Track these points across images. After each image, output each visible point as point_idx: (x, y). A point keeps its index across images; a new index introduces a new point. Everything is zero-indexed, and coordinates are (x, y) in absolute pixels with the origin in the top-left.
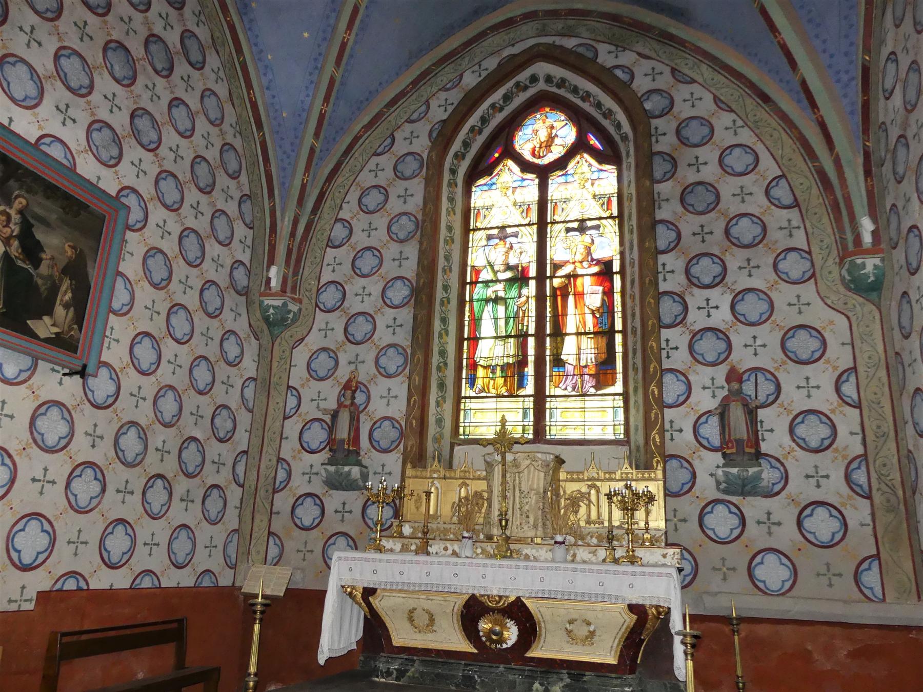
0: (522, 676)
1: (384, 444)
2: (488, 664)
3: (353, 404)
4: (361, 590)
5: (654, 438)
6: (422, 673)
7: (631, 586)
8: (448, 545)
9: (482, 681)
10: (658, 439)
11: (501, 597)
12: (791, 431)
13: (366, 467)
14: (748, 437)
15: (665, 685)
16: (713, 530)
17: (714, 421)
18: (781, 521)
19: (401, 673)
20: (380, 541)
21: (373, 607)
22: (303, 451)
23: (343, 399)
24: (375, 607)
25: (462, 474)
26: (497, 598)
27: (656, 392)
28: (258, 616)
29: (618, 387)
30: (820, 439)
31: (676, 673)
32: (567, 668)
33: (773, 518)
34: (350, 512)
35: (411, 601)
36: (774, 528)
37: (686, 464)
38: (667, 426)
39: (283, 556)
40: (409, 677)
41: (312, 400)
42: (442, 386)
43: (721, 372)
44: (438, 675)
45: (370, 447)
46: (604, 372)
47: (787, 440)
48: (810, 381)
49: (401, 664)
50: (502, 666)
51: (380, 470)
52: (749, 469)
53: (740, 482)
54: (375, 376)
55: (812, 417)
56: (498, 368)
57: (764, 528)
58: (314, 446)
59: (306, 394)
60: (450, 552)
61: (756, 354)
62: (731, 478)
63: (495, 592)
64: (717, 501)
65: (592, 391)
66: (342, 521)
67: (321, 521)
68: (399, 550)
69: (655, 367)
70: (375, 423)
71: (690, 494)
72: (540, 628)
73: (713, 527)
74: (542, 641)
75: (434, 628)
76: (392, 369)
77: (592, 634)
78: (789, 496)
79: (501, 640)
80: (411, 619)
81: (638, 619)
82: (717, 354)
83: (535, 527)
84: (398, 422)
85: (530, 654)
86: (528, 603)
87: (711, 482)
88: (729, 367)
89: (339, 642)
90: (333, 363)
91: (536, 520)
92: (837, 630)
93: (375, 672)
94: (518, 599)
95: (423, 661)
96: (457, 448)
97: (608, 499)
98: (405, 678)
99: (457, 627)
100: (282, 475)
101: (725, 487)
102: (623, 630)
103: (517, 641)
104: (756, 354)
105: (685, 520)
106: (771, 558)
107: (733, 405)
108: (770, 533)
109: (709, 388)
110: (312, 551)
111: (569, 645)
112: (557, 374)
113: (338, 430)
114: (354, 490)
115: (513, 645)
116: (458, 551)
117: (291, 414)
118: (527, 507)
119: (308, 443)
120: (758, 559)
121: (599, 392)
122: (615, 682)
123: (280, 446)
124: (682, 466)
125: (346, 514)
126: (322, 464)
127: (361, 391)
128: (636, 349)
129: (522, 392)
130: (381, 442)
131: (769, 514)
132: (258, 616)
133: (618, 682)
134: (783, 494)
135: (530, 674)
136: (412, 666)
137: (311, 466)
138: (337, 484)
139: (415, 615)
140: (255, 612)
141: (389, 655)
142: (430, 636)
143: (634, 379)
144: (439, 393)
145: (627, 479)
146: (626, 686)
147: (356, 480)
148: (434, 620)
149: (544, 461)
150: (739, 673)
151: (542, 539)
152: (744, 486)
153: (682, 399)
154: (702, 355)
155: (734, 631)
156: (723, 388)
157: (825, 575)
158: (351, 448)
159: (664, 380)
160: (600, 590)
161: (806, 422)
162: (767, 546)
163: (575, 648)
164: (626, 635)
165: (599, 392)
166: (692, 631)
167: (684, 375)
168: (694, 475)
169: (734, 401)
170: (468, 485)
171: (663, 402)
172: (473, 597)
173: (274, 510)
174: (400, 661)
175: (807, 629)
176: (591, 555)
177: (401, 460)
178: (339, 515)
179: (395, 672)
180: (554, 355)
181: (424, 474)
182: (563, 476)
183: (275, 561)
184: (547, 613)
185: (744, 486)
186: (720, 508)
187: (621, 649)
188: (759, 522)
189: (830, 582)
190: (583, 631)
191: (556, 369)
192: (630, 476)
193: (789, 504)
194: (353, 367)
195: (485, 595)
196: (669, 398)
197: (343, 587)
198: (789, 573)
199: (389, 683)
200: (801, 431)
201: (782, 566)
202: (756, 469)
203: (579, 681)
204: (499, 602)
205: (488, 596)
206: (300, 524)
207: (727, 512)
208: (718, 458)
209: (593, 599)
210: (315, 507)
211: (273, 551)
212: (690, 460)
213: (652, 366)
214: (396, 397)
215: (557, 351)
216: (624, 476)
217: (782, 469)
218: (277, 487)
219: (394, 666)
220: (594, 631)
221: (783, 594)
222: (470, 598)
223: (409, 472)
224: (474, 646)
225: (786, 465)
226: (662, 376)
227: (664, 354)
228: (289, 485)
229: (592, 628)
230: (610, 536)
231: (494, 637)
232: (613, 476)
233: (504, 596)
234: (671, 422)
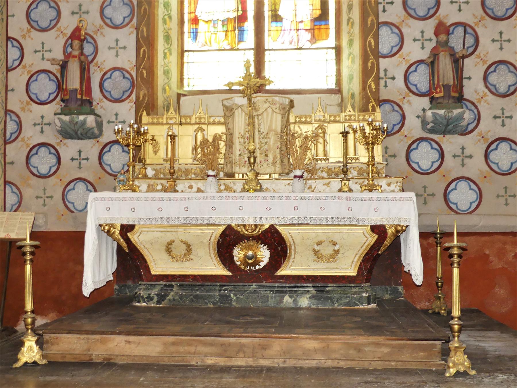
0: (273, 291)
1: (116, 94)
2: (241, 284)
3: (82, 54)
4: (119, 228)
5: (370, 85)
6: (181, 297)
7: (376, 209)
8: (193, 184)
9: (238, 298)
10: (373, 86)
11: (256, 226)
12: (485, 78)
13: (100, 117)
14: (454, 82)
15: (387, 289)
16: (418, 163)
17: (423, 70)
18: (473, 155)
19: (161, 298)
20: (133, 181)
21: (131, 242)
22: (32, 102)
23: (69, 50)
24: (133, 242)
25: (198, 120)
26: (253, 227)
27: (373, 44)
28: (28, 257)
29: (331, 41)
30: (507, 86)
31: (414, 279)
32: (313, 282)
33: (467, 152)
34: (87, 159)
35: (168, 234)
36: (466, 161)
37: (397, 108)
38: (382, 74)
39: (23, 203)
40: (169, 300)
41: (36, 52)
42: (167, 38)
43: (430, 26)
44: (197, 297)
45: (102, 97)
46: (318, 27)
47: (481, 86)
48: (503, 35)
49: (161, 290)
50: (254, 284)
51: (113, 119)
52: (454, 111)
53: (445, 122)
54: (101, 27)
55: (502, 67)
56: (220, 23)
57: (459, 160)
58: (44, 97)
59: (29, 46)
60: (195, 189)
61: (460, 10)
62: (438, 118)
63: (251, 222)
64: (421, 139)
65: (308, 45)
66: (80, 168)
67: (58, 169)
68: (145, 190)
69: (372, 20)
70: (105, 74)
71: (400, 133)
72: (290, 250)
73: (417, 161)
74: (291, 260)
75: (191, 257)
76: (118, 19)
77: (337, 252)
78: (480, 134)
79: (257, 262)
80: (169, 251)
81: (378, 237)
82: (427, 9)
83: (274, 164)
84: (128, 72)
85: (279, 273)
86: (280, 229)
87: (418, 123)
88: (437, 21)
89: (99, 277)
90: (54, 14)
91: (275, 158)
92: (509, 238)
93: (137, 298)
94: (272, 227)
95: (180, 285)
96: (182, 99)
97: (343, 136)
98: (166, 301)
99: (213, 255)
100: (11, 127)
101: (432, 127)
102: (364, 247)
103: (268, 263)
104: (460, 10)
105: (394, 156)
106: (463, 185)
107: (442, 55)
108: (463, 165)
109: (419, 40)
110: (52, 197)
111: (315, 263)
112: (276, 28)
113: (68, 78)
114: (89, 138)
115: (265, 266)
116: (202, 188)
117: (14, 67)
118: (266, 147)
119: (36, 94)
120: (453, 186)
121: (314, 46)
122: (354, 290)
123: (6, 99)
124: (393, 110)
125: (83, 162)
126: (56, 114)
127: (88, 42)
128: (352, 4)
129: (242, 46)
130: (112, 92)
131: (463, 149)
132: (28, 257)
133: (357, 289)
134: (475, 132)
135: (279, 289)
136: (172, 290)
137: (42, 117)
138: (73, 133)
139: (173, 247)
140: (24, 254)
141: (148, 283)
142: (187, 264)
143: (349, 33)
144: (166, 45)
145: (350, 120)
146: (364, 292)
147: (93, 128)
148: (191, 250)
149: (281, 104)
150: (439, 275)
151: (280, 174)
152: (447, 125)
153: (395, 50)
154: (414, 9)
155: (437, 244)
156: (430, 40)
157: (503, 196)
158: (84, 98)
159: (380, 33)
160: (349, 215)
161: (498, 71)
162: (460, 175)
163: (319, 265)
164: (366, 251)
165: (314, 46)
166: (458, 244)
167: (398, 28)
168: (403, 117)
169: (442, 51)
170: (204, 130)
171: (379, 52)
172: (229, 228)
173: (8, 160)
174: (159, 287)
175: (484, 239)
176: (325, 186)
177: (133, 110)
178: (76, 163)
179: (156, 297)
180: (272, 11)
181: (161, 120)
182: (292, 119)
183: (15, 207)
184: (298, 238)
185: (447, 125)
186: (424, 145)
187: (361, 263)
188: (455, 156)
189: (507, 202)
190: (327, 250)
191: (274, 24)
192: (353, 118)
193: (479, 141)
194: (76, 17)
195: (241, 225)
196: (384, 49)
197: (100, 225)
198: (475, 196)
199: (151, 307)
200: (493, 78)
201: (471, 191)
202: (459, 111)
203: (324, 291)
204: (255, 230)
205: (245, 226)
206: (36, 173)
207: (430, 148)
208: (425, 102)
209: (343, 223)
210: (50, 156)
211: (12, 199)
212: (401, 104)
213: (370, 20)
214: (125, 48)
215: (275, 6)
216: (347, 118)
217: (475, 111)
218: (8, 138)
219: (154, 292)
220: (339, 250)
221: (471, 213)
222: (226, 228)
223: (145, 119)
224: (228, 270)
225: (479, 107)
226: (378, 28)
227: (381, 8)
228: (22, 136)
229: (337, 248)
230: (345, 169)
231: (250, 261)
232: (338, 118)
233: (259, 225)
234: (386, 70)
